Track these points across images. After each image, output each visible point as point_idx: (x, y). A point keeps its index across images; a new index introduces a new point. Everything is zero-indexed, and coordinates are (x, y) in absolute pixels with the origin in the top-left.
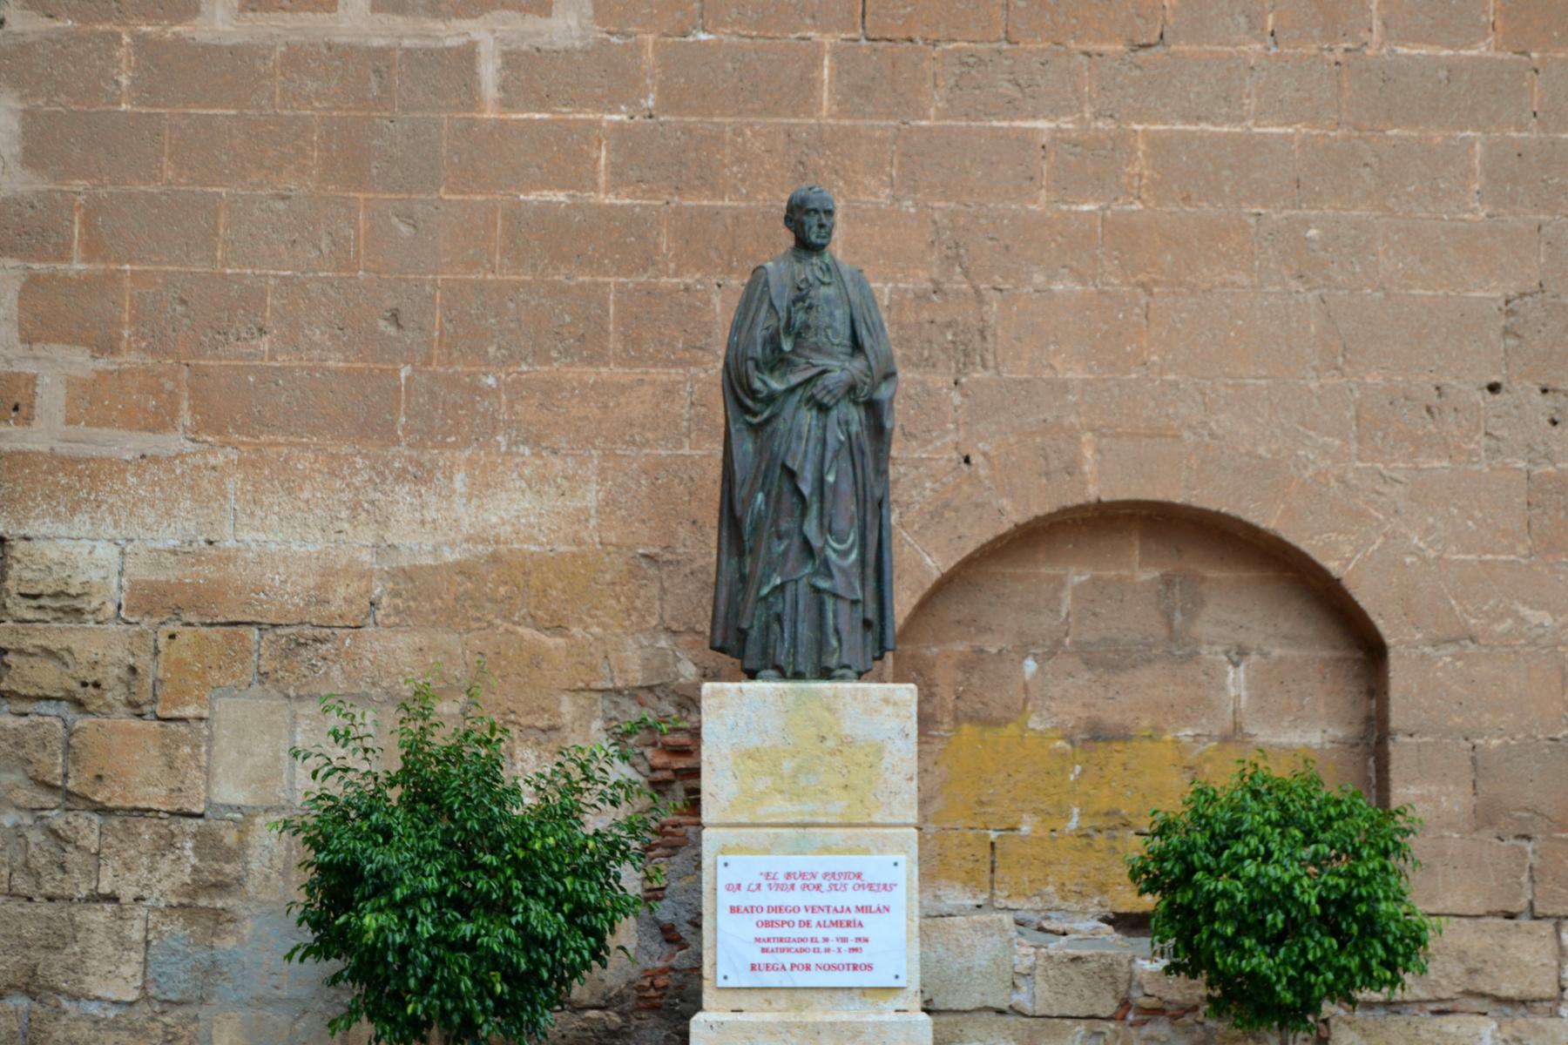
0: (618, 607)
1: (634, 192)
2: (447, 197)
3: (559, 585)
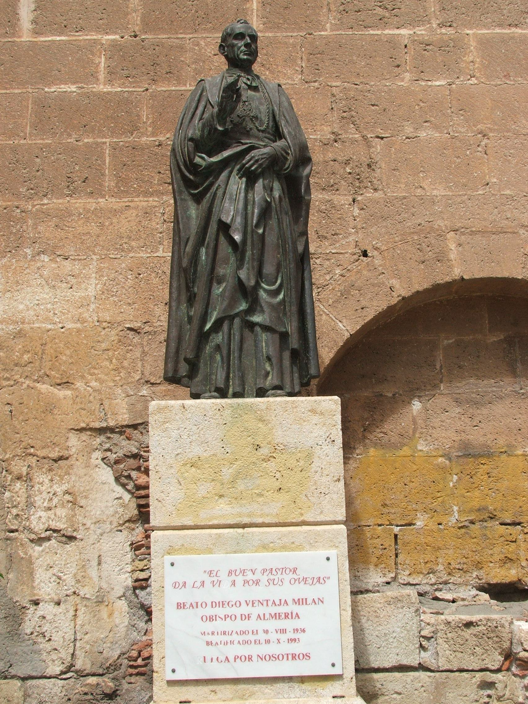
0: (111, 367)
1: (124, 84)
3: (68, 352)
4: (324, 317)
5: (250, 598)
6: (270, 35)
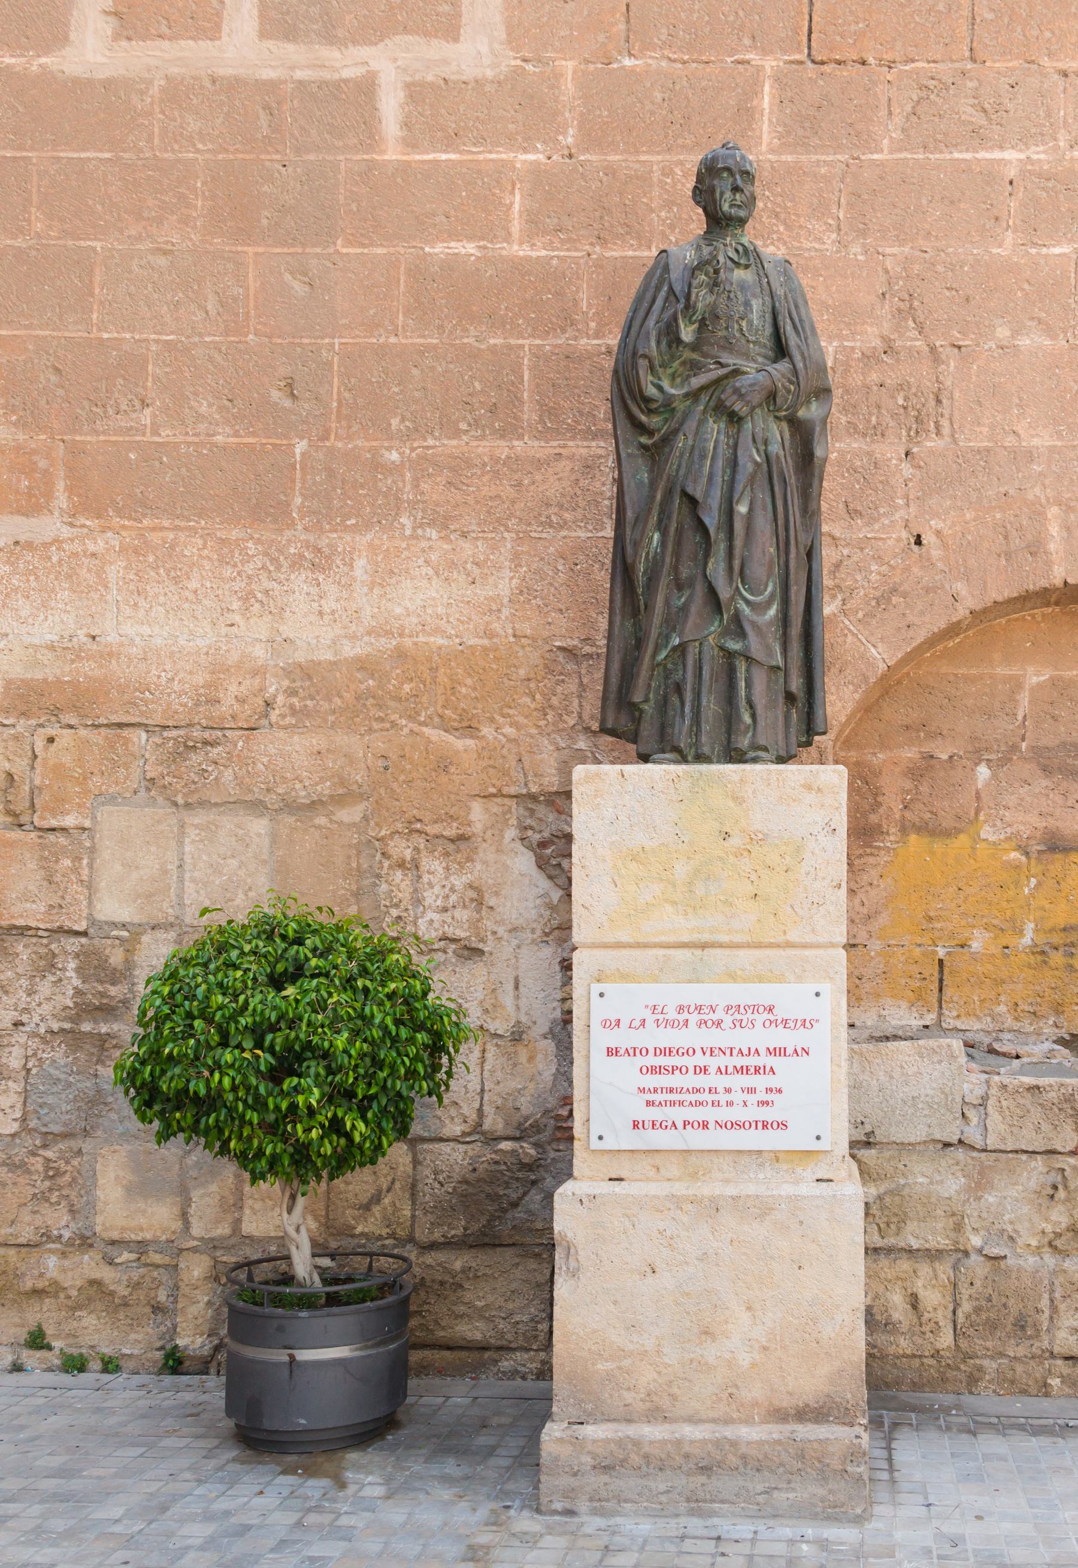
0: (533, 706)
2: (344, 251)
3: (469, 681)
4: (850, 638)
5: (707, 1045)
6: (790, 158)
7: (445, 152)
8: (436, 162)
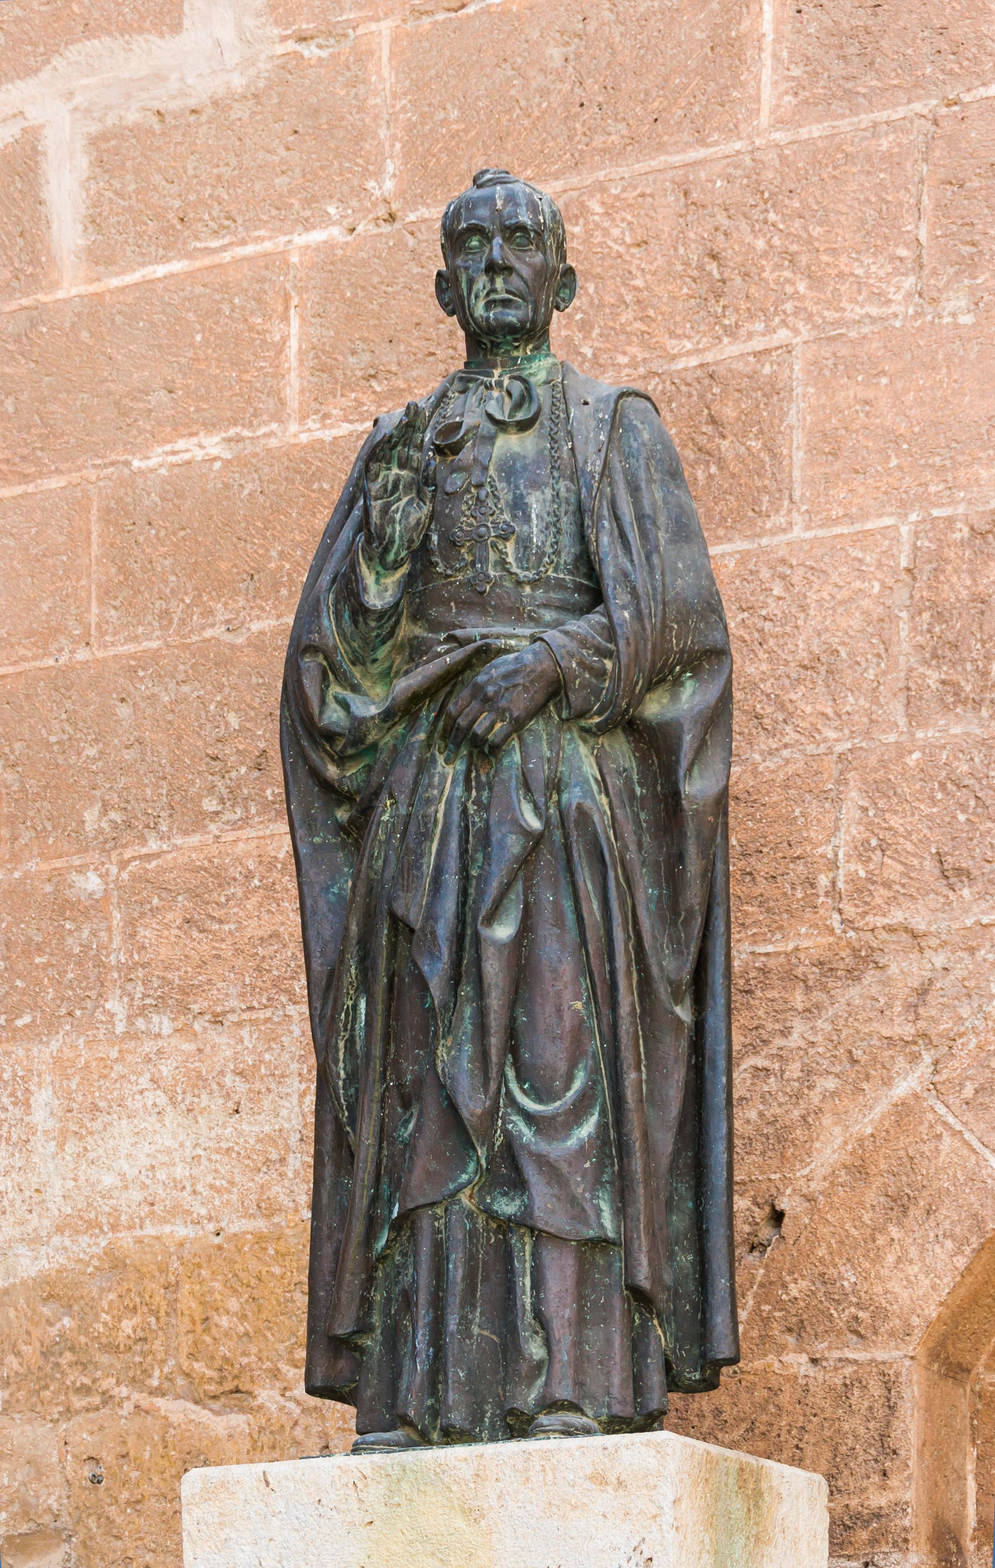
3: (233, 1304)
6: (816, 131)
7: (164, 260)
8: (149, 283)
